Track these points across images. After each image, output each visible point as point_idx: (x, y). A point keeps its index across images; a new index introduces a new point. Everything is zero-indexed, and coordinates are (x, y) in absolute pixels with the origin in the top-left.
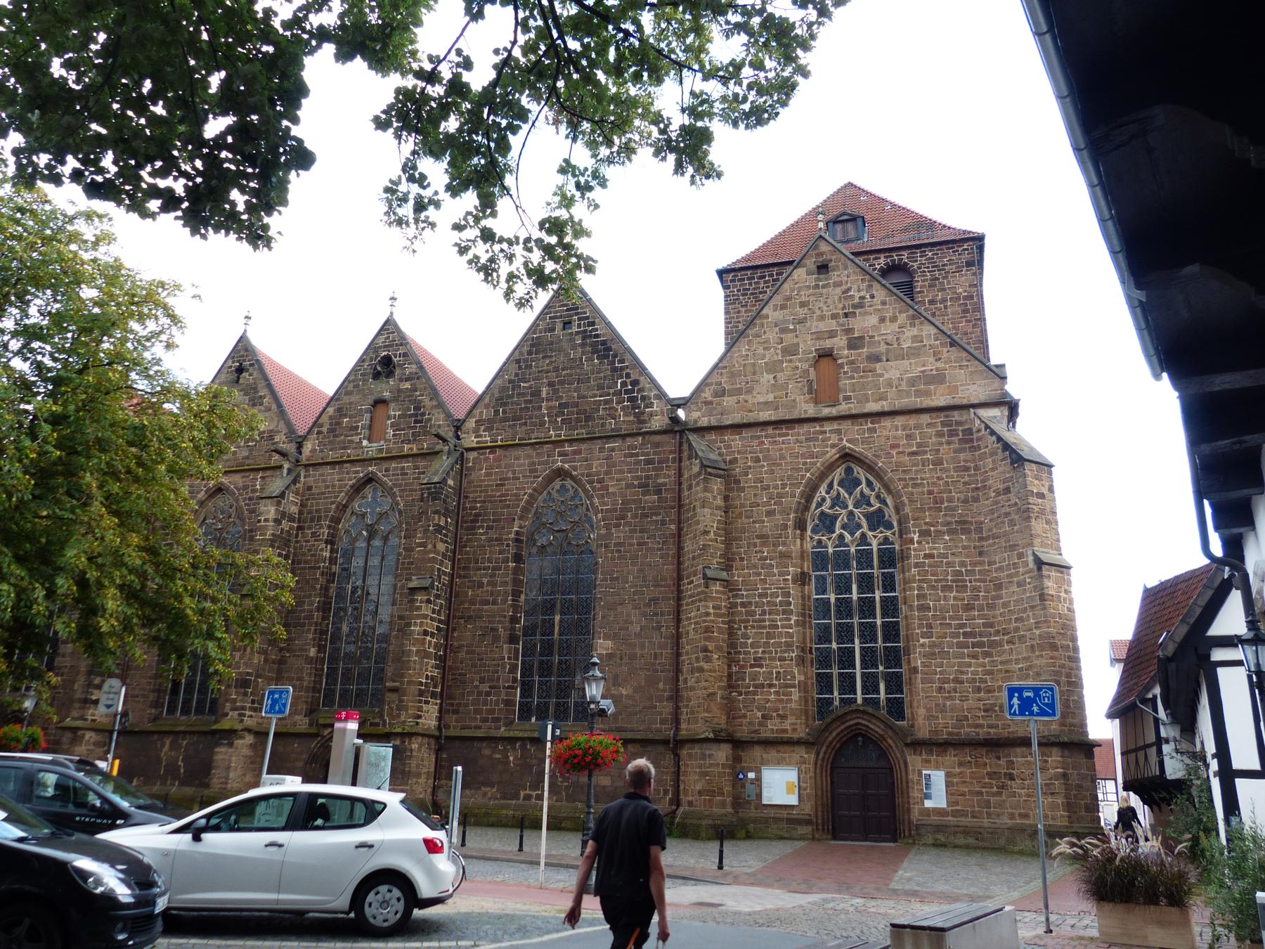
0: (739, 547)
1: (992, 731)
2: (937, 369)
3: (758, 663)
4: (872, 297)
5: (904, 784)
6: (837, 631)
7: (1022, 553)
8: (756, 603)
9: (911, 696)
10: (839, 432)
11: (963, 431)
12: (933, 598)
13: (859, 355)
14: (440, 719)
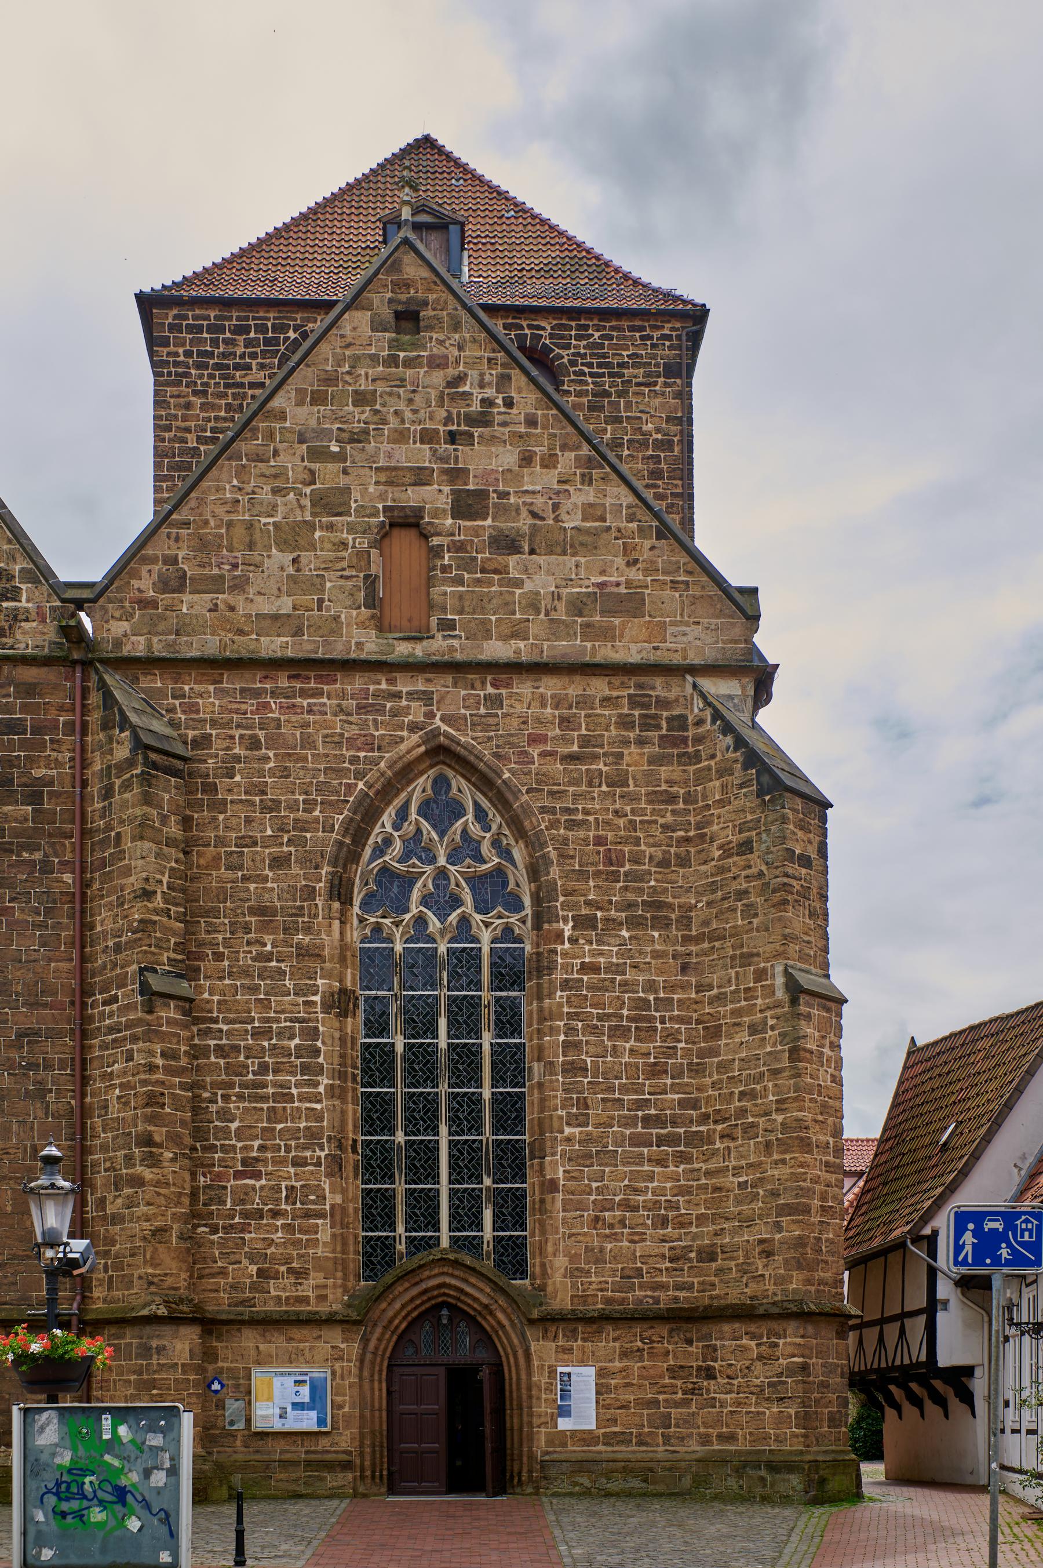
0: (213, 930)
1: (681, 1294)
2: (629, 584)
3: (250, 1168)
4: (509, 403)
5: (524, 1391)
6: (405, 1109)
7: (764, 971)
8: (248, 1048)
9: (543, 1232)
10: (426, 697)
11: (670, 720)
12: (592, 1049)
13: (476, 532)
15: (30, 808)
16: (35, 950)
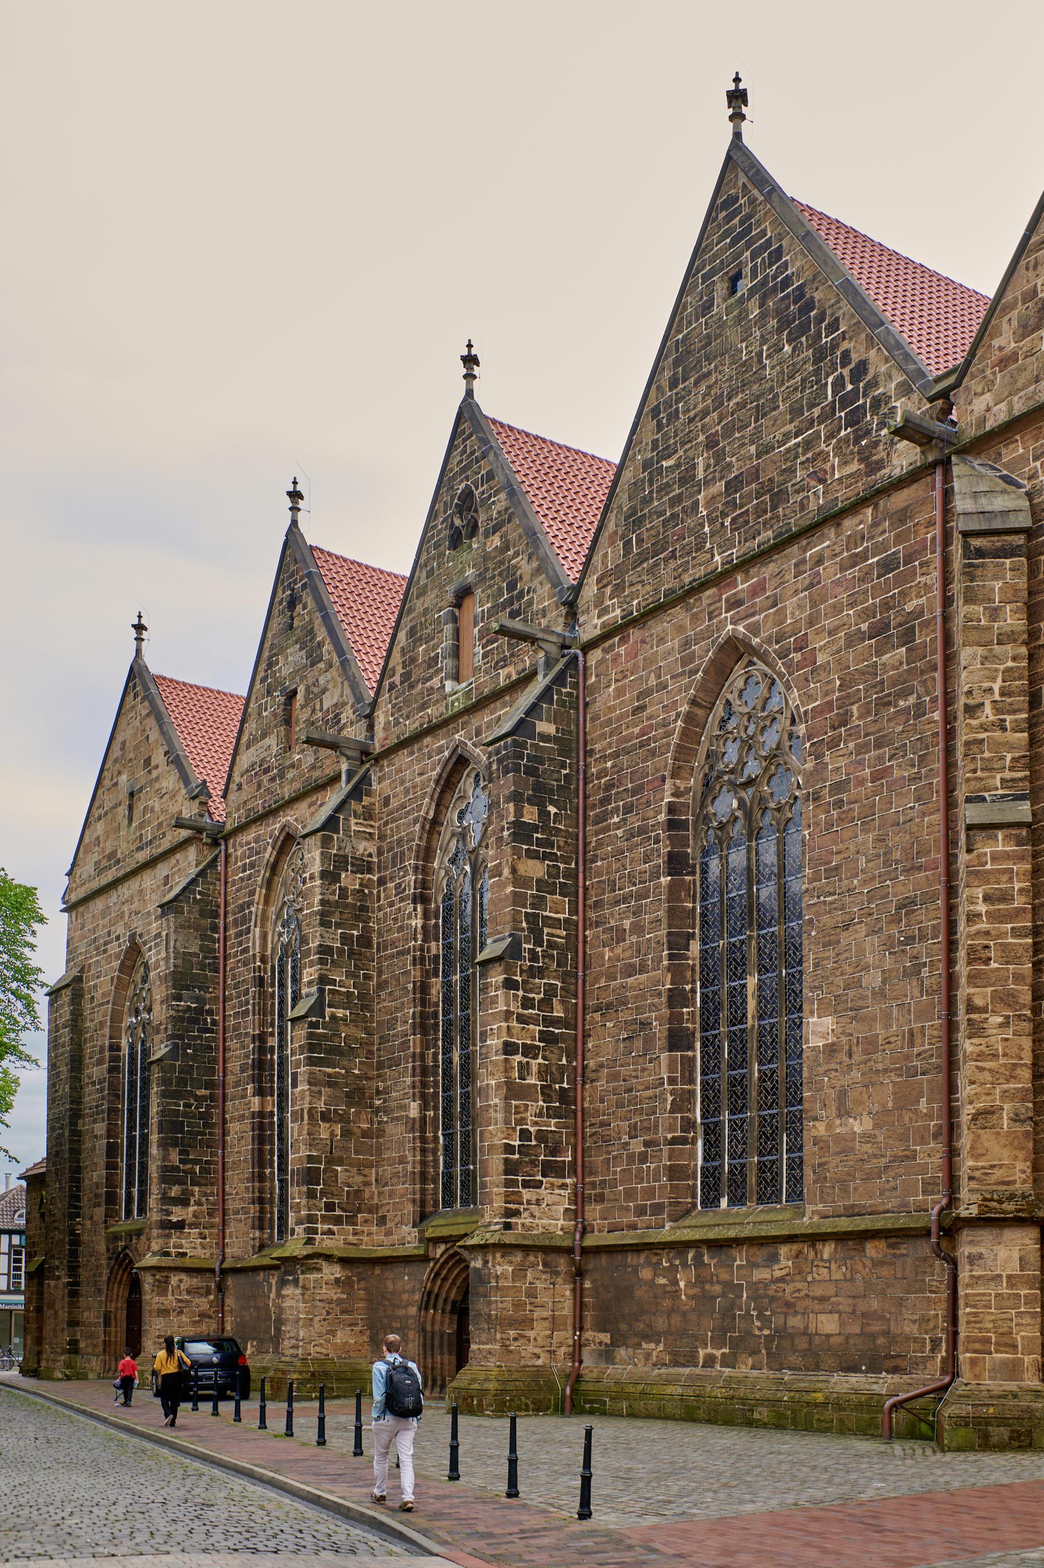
14: (576, 1213)
15: (904, 649)
16: (911, 808)
